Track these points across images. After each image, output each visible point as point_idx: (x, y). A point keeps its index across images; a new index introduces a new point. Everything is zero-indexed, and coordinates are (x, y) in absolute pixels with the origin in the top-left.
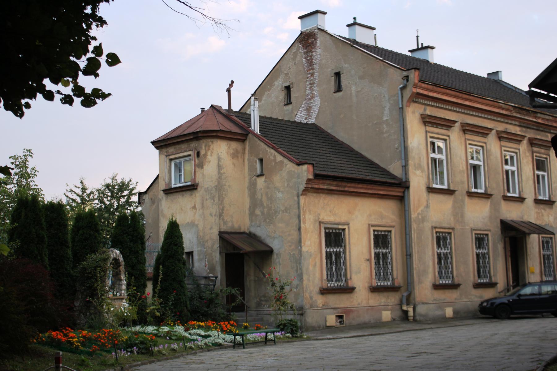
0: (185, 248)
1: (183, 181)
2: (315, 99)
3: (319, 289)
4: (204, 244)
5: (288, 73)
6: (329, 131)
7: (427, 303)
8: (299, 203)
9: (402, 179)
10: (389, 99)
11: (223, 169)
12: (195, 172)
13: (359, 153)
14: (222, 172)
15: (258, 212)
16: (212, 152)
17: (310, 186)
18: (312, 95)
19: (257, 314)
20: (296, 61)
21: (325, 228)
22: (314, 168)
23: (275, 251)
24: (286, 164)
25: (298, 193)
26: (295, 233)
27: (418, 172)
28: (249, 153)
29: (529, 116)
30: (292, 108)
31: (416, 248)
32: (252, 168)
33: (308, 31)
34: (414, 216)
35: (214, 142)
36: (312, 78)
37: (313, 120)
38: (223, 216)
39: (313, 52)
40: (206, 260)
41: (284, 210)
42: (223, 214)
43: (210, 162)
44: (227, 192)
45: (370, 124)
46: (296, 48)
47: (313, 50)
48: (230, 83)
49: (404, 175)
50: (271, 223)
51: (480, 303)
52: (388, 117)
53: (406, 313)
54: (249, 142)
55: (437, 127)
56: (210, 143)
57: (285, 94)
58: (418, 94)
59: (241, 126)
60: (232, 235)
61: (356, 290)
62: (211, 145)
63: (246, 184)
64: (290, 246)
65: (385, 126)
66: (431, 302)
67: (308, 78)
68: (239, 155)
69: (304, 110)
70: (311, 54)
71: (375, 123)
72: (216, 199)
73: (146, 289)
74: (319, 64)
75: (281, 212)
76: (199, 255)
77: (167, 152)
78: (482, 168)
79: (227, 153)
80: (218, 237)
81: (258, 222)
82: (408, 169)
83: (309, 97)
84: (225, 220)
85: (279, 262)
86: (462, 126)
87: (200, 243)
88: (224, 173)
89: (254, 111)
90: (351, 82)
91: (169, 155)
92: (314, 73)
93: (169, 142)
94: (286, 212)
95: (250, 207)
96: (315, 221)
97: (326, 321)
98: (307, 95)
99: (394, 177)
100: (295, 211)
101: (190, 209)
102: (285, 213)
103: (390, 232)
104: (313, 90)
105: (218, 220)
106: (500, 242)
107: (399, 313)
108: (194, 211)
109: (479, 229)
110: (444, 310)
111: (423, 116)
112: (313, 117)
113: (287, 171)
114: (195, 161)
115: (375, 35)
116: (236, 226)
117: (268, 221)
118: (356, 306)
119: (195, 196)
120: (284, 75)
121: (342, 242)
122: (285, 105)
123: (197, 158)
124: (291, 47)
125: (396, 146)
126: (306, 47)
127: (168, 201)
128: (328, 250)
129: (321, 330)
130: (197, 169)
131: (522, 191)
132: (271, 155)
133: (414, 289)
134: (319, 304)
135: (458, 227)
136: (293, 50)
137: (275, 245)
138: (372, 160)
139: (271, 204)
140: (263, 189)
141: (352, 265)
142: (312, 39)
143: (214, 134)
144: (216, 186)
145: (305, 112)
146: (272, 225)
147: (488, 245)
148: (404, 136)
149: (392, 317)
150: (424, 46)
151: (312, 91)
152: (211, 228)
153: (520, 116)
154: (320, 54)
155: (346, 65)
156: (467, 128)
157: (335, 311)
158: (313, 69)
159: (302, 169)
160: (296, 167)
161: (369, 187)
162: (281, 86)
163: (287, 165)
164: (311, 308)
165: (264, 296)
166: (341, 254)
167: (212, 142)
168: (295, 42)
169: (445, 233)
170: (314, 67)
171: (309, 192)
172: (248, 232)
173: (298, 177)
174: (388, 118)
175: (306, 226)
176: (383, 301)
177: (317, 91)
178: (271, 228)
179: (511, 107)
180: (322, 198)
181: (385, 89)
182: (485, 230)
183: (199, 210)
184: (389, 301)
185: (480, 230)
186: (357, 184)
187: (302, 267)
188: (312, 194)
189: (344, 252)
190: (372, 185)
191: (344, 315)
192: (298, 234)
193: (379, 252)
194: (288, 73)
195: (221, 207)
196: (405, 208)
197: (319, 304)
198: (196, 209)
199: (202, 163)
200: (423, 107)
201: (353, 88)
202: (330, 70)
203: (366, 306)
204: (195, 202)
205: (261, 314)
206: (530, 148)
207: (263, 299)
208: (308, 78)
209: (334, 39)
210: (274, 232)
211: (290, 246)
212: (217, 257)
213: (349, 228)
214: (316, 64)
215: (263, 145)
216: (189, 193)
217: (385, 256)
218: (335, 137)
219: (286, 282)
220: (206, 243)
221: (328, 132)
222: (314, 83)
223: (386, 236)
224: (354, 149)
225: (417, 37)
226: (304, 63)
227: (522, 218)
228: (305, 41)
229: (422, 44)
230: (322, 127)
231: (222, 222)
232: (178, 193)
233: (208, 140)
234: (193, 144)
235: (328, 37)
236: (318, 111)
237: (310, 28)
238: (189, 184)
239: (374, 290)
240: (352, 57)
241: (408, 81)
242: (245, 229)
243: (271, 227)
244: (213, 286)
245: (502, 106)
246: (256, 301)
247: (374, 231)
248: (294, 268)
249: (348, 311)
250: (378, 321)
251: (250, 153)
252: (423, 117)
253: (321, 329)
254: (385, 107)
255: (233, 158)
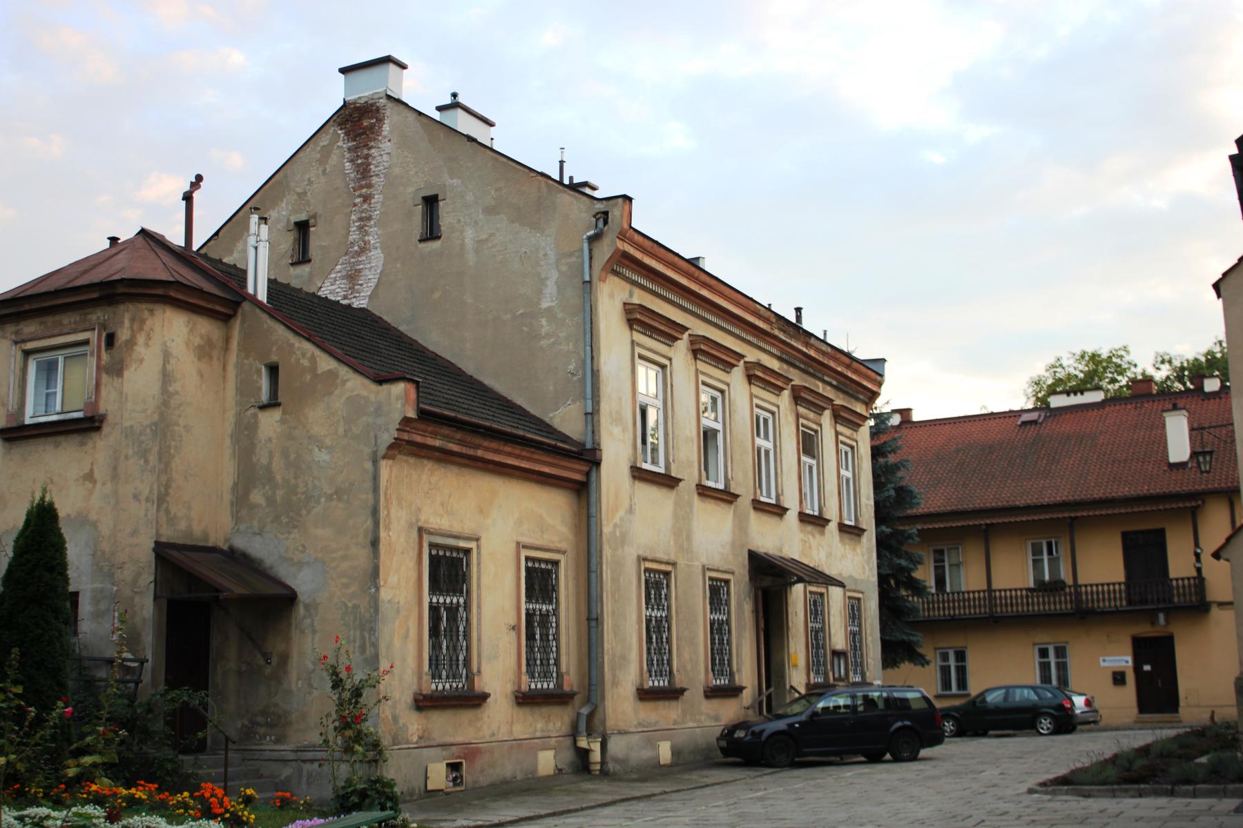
0: (71, 581)
1: (58, 408)
2: (370, 254)
3: (412, 696)
4: (113, 573)
5: (305, 193)
6: (402, 328)
7: (626, 733)
8: (376, 478)
9: (583, 445)
10: (558, 261)
11: (175, 381)
12: (98, 385)
13: (476, 380)
14: (171, 389)
15: (257, 497)
16: (149, 338)
17: (406, 436)
18: (363, 245)
19: (244, 760)
20: (327, 167)
21: (432, 545)
22: (418, 392)
23: (303, 597)
24: (345, 378)
25: (375, 453)
26: (362, 555)
27: (617, 431)
28: (239, 350)
29: (797, 340)
30: (310, 273)
31: (609, 603)
32: (245, 387)
33: (362, 101)
34: (607, 530)
35: (155, 312)
36: (365, 206)
37: (362, 302)
38: (168, 502)
39: (372, 147)
40: (116, 614)
41: (332, 495)
42: (168, 499)
43: (141, 361)
44: (181, 441)
45: (508, 316)
46: (328, 137)
47: (372, 144)
48: (194, 180)
49: (590, 433)
50: (295, 527)
51: (720, 731)
52: (552, 301)
53: (584, 754)
54: (243, 323)
55: (650, 337)
56: (146, 313)
57: (295, 240)
58: (626, 256)
59: (224, 283)
60: (189, 554)
61: (488, 700)
62: (146, 319)
63: (229, 427)
64: (346, 586)
65: (544, 322)
66: (634, 730)
67: (355, 205)
68: (215, 353)
69: (343, 278)
70: (366, 152)
71: (521, 314)
72: (151, 458)
73: (902, 665)
74: (386, 175)
75: (323, 500)
76: (96, 601)
77: (16, 333)
78: (720, 437)
79: (187, 343)
80: (154, 555)
81: (255, 523)
82: (599, 421)
83: (356, 248)
84: (173, 512)
85: (312, 625)
86: (692, 343)
87: (101, 569)
88: (177, 393)
89: (256, 248)
90: (462, 220)
91: (24, 341)
92: (370, 194)
93: (27, 307)
94: (339, 499)
95: (235, 485)
96: (411, 525)
97: (426, 778)
98: (351, 243)
99: (565, 438)
100: (364, 496)
101: (77, 480)
102: (334, 503)
103: (556, 563)
104: (367, 234)
105: (155, 511)
106: (748, 599)
107: (568, 756)
108: (90, 485)
109: (716, 568)
110: (657, 748)
111: (628, 307)
112: (362, 294)
113: (347, 396)
114: (99, 358)
115: (492, 139)
116: (197, 530)
117: (284, 519)
118: (488, 739)
119: (94, 448)
120: (295, 197)
121: (464, 581)
122: (292, 264)
123: (106, 350)
124: (318, 135)
125: (571, 367)
126: (355, 136)
127: (11, 460)
128: (435, 600)
129: (416, 800)
130: (105, 378)
131: (782, 494)
132: (304, 355)
133: (603, 698)
134: (412, 735)
135: (682, 562)
136: (322, 141)
137: (302, 582)
138: (509, 398)
139: (296, 477)
140: (274, 441)
141: (483, 638)
142: (372, 118)
143: (160, 291)
144: (155, 424)
145: (343, 281)
146: (296, 530)
147: (728, 603)
148: (591, 347)
149: (556, 766)
150: (575, 181)
151: (364, 236)
152: (134, 533)
153: (784, 338)
154: (388, 154)
155: (455, 181)
156: (703, 347)
157: (444, 753)
158: (370, 186)
159: (389, 394)
160: (373, 387)
161: (524, 454)
162: (286, 220)
163: (347, 380)
164: (394, 745)
165: (264, 713)
166: (461, 609)
167: (151, 311)
168: (329, 124)
169: (660, 572)
170: (374, 182)
171: (400, 453)
172: (225, 548)
173: (378, 411)
174: (553, 304)
175: (390, 536)
176: (539, 726)
177: (376, 237)
178: (295, 539)
179: (773, 315)
180: (426, 470)
181: (548, 239)
182: (725, 572)
183: (104, 484)
184: (551, 726)
185: (717, 571)
186: (502, 443)
187: (377, 639)
188: (405, 458)
189: (467, 606)
190: (533, 450)
191: (464, 761)
192: (372, 555)
193: (534, 610)
194: (305, 193)
195: (164, 478)
196: (588, 509)
197: (412, 735)
198: (94, 482)
199: (122, 361)
200: (628, 286)
201: (469, 234)
202: (414, 189)
203: (506, 739)
204: (92, 464)
205: (253, 759)
206: (794, 406)
207: (260, 719)
208: (355, 205)
209: (425, 120)
210: (300, 548)
211: (346, 586)
212: (146, 608)
213: (478, 547)
214: (377, 175)
215: (280, 331)
216: (76, 438)
217: (545, 617)
218: (416, 342)
219: (367, 677)
220: (119, 571)
221: (399, 331)
222: (369, 218)
223: (549, 572)
224: (464, 372)
225: (562, 162)
226: (347, 172)
227: (781, 550)
228: (352, 122)
229: (571, 178)
230: (385, 318)
231: (163, 519)
232: (43, 440)
233: (139, 305)
234: (97, 315)
235: (412, 117)
236: (376, 280)
237: (366, 94)
238: (79, 415)
239: (525, 699)
240: (470, 165)
241: (606, 222)
242: (217, 539)
243: (292, 536)
244: (132, 685)
245: (759, 310)
246: (239, 726)
247: (527, 559)
248: (355, 641)
249: (472, 751)
250: (530, 776)
251: (245, 349)
252: (629, 309)
253: (415, 798)
254: (547, 279)
255: (199, 359)
